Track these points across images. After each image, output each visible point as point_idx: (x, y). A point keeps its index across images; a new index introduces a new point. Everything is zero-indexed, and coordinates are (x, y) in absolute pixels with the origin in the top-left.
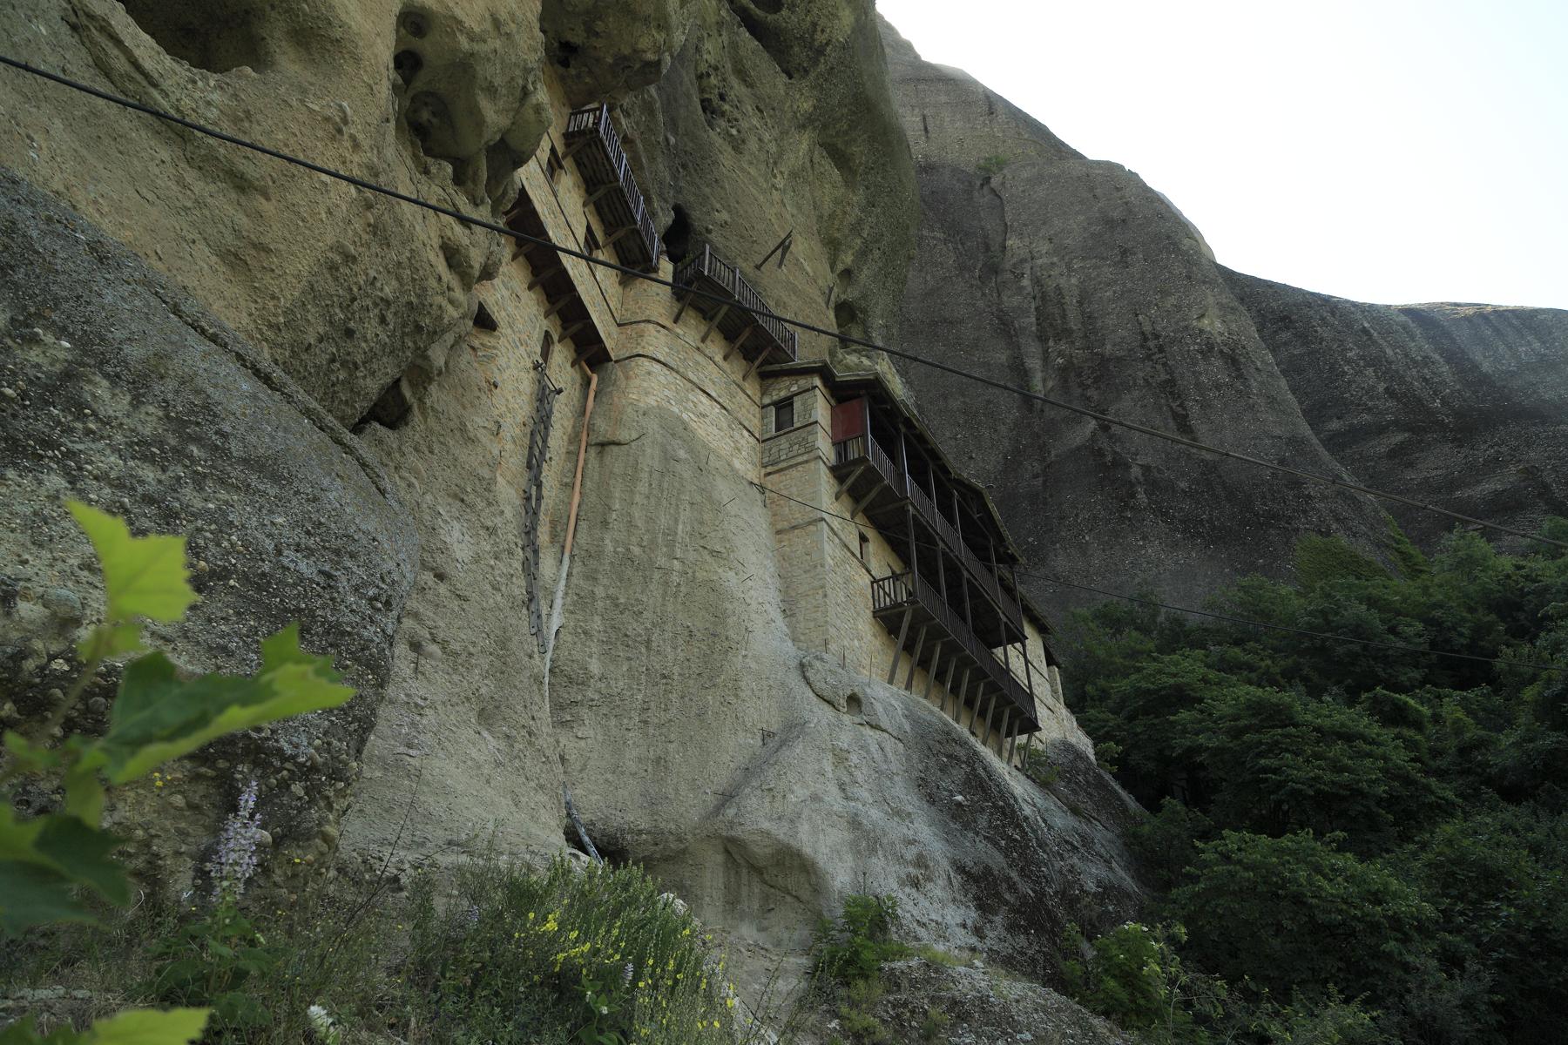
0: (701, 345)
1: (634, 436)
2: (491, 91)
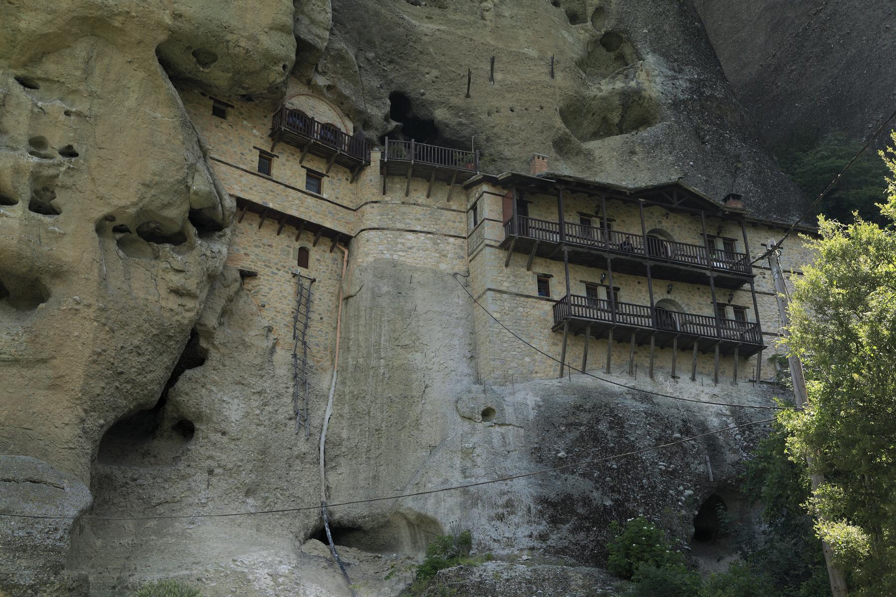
0: (406, 199)
1: (358, 288)
2: (165, 206)
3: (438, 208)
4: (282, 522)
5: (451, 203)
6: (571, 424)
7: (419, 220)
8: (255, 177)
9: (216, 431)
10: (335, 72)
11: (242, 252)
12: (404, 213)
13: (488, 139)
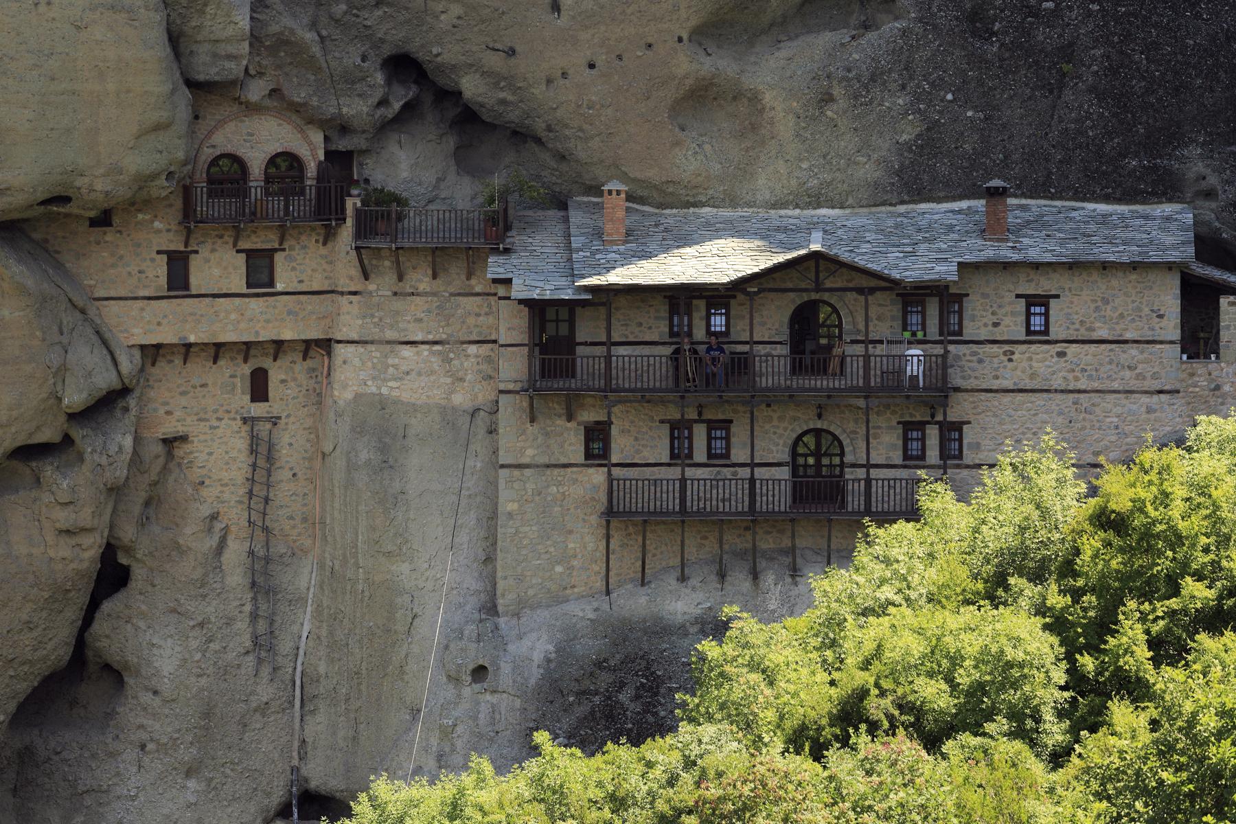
3: (452, 295)
4: (230, 810)
5: (473, 282)
6: (584, 693)
7: (420, 320)
8: (164, 303)
9: (147, 689)
10: (279, 67)
11: (161, 412)
12: (397, 313)
13: (549, 129)
